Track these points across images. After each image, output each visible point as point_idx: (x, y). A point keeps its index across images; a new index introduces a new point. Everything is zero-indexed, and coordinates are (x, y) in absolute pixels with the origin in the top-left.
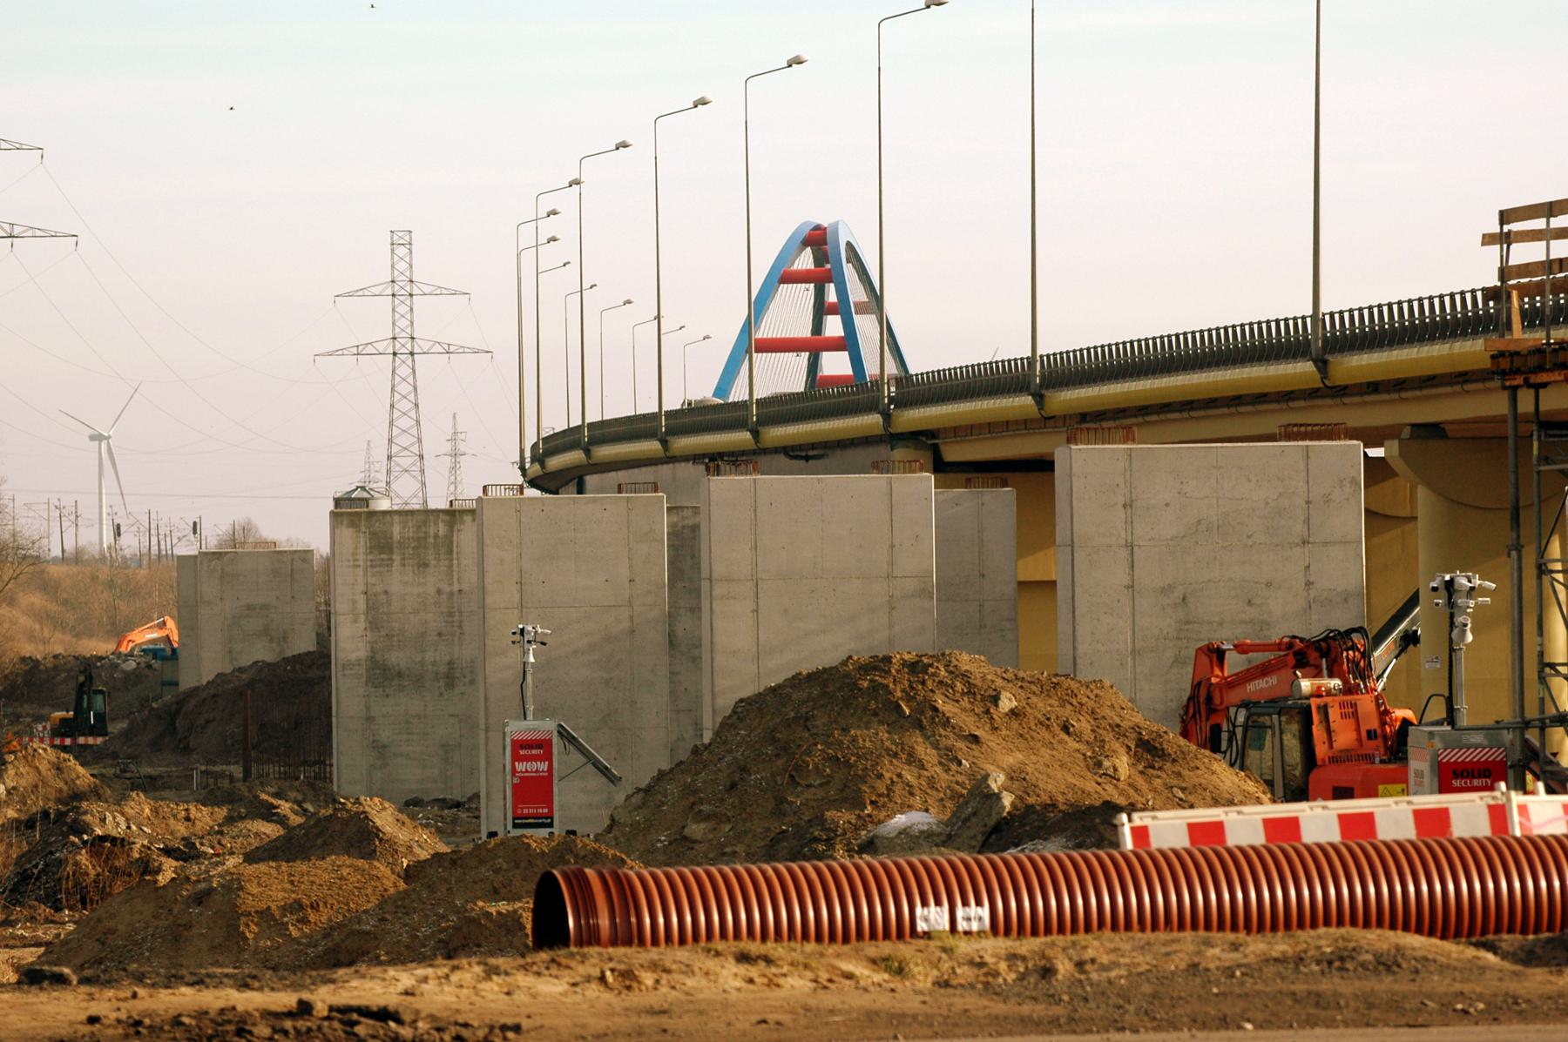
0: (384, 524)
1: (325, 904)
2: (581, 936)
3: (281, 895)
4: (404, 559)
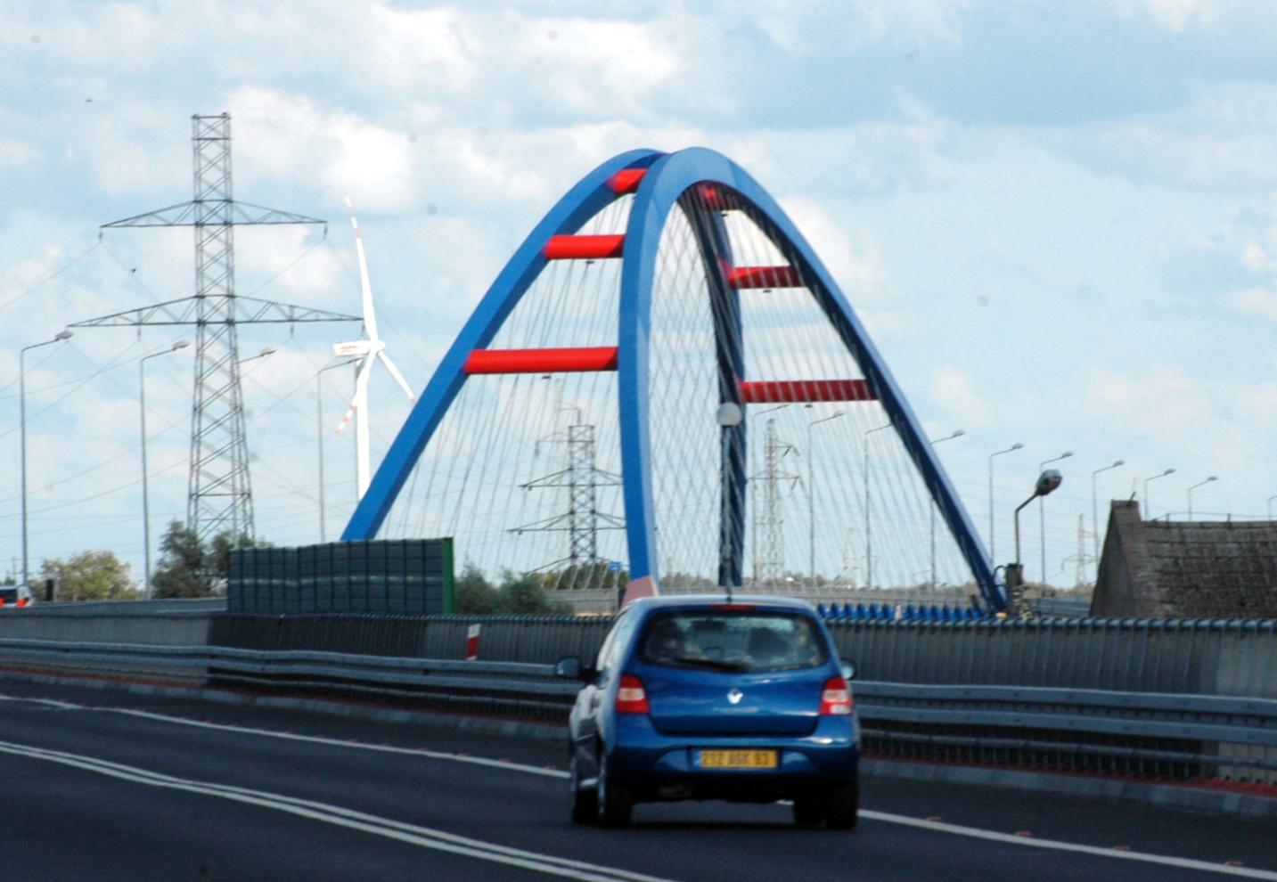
2: (1209, 528)
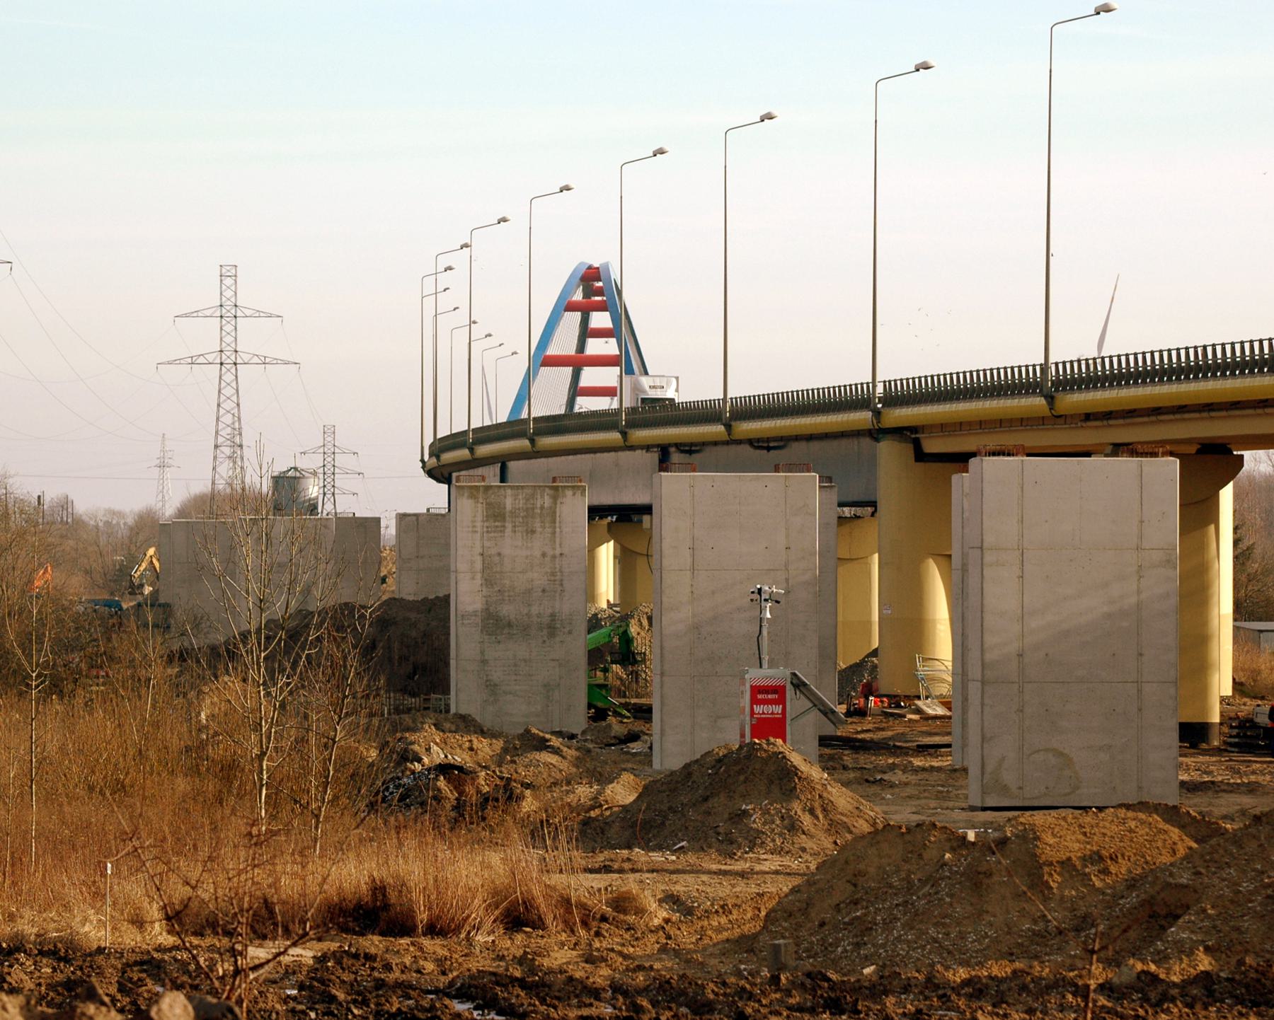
1: (1123, 855)
3: (1076, 846)
4: (515, 526)
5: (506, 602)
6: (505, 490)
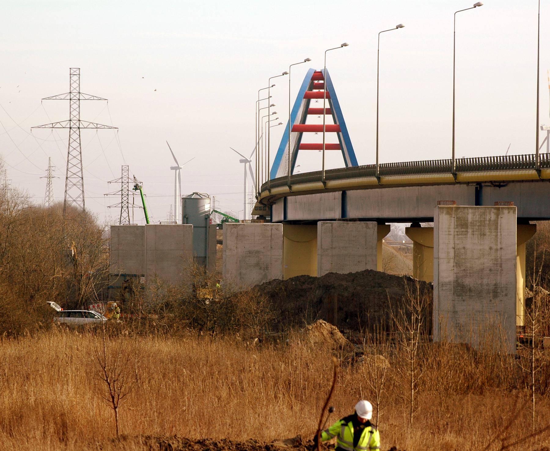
0: (464, 213)
5: (468, 276)
6: (467, 210)
